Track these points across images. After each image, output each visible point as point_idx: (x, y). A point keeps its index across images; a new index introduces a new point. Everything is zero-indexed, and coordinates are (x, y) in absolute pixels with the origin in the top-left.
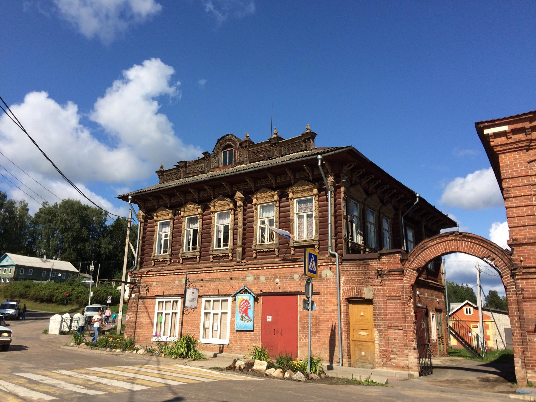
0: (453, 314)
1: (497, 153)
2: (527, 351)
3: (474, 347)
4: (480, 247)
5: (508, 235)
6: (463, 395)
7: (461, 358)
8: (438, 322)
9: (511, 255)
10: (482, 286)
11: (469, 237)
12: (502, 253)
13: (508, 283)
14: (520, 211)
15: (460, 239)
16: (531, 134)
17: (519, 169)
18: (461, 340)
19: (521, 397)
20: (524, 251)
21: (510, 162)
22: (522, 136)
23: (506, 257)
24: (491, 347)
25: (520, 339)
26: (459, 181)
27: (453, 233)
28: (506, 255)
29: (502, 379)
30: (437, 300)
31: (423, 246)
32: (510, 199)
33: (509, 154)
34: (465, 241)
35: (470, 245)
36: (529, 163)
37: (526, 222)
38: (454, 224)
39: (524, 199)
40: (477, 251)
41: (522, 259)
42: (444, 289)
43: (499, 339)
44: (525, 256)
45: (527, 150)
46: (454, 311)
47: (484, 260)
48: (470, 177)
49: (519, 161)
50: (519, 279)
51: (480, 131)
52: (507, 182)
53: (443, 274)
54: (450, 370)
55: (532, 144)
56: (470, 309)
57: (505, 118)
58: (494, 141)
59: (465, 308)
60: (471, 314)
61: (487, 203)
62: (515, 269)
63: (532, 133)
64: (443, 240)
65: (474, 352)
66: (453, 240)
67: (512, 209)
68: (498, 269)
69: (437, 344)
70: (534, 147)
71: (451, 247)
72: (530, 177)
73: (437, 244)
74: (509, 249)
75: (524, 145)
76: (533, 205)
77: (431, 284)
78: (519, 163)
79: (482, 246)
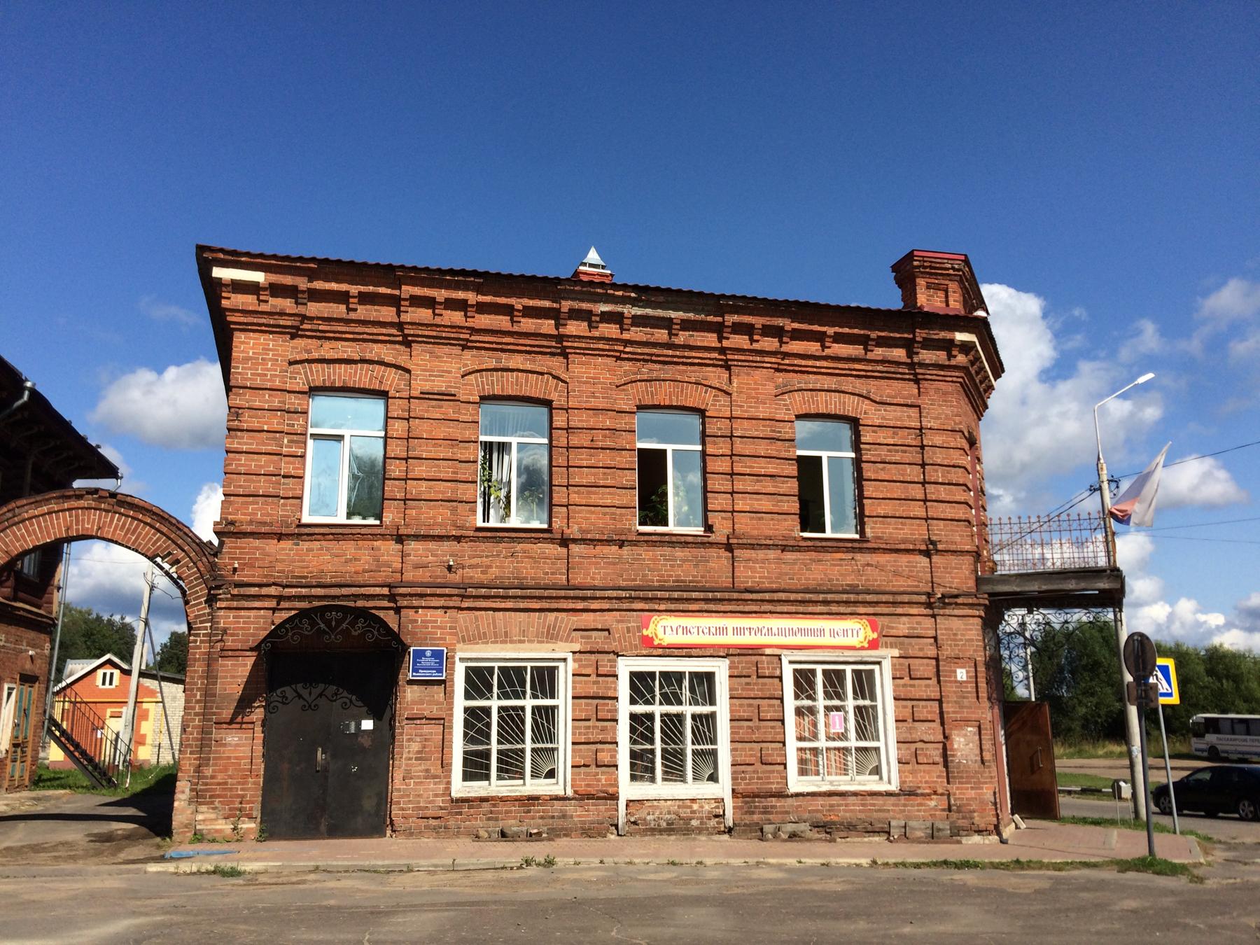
0: (64, 689)
1: (232, 326)
2: (207, 765)
3: (101, 764)
4: (153, 531)
5: (219, 511)
6: (37, 879)
7: (62, 792)
8: (20, 708)
9: (215, 555)
10: (151, 622)
11: (132, 506)
12: (197, 548)
13: (197, 617)
14: (253, 463)
15: (110, 508)
16: (306, 304)
17: (269, 373)
18: (72, 749)
19: (170, 867)
20: (245, 548)
21: (253, 353)
22: (287, 304)
23: (204, 559)
24: (144, 760)
25: (197, 739)
26: (145, 376)
27: (96, 491)
28: (205, 555)
29: (144, 830)
30: (31, 653)
31: (10, 515)
32: (239, 434)
33: (256, 335)
34: (120, 513)
35: (131, 524)
36: (291, 363)
37: (260, 487)
38: (110, 471)
39: (267, 439)
40: (143, 540)
41: (236, 565)
42: (55, 625)
43: (165, 742)
44: (245, 558)
45: (293, 337)
46: (69, 681)
47: (155, 563)
48: (172, 372)
49: (273, 355)
50: (221, 608)
51: (204, 268)
52: (239, 395)
53: (59, 588)
54: (22, 825)
55: (305, 326)
56: (112, 675)
57: (261, 256)
58: (229, 298)
59: (100, 673)
60: (113, 687)
61: (200, 437)
62: (218, 587)
63: (309, 304)
64: (66, 506)
65: (99, 773)
66: (91, 508)
67: (237, 456)
68: (183, 585)
69: (8, 762)
70: (307, 333)
71: (83, 525)
72: (287, 395)
73: (50, 513)
74: (216, 542)
75: (289, 323)
76: (281, 454)
77: (21, 613)
78: (270, 360)
79: (158, 530)
